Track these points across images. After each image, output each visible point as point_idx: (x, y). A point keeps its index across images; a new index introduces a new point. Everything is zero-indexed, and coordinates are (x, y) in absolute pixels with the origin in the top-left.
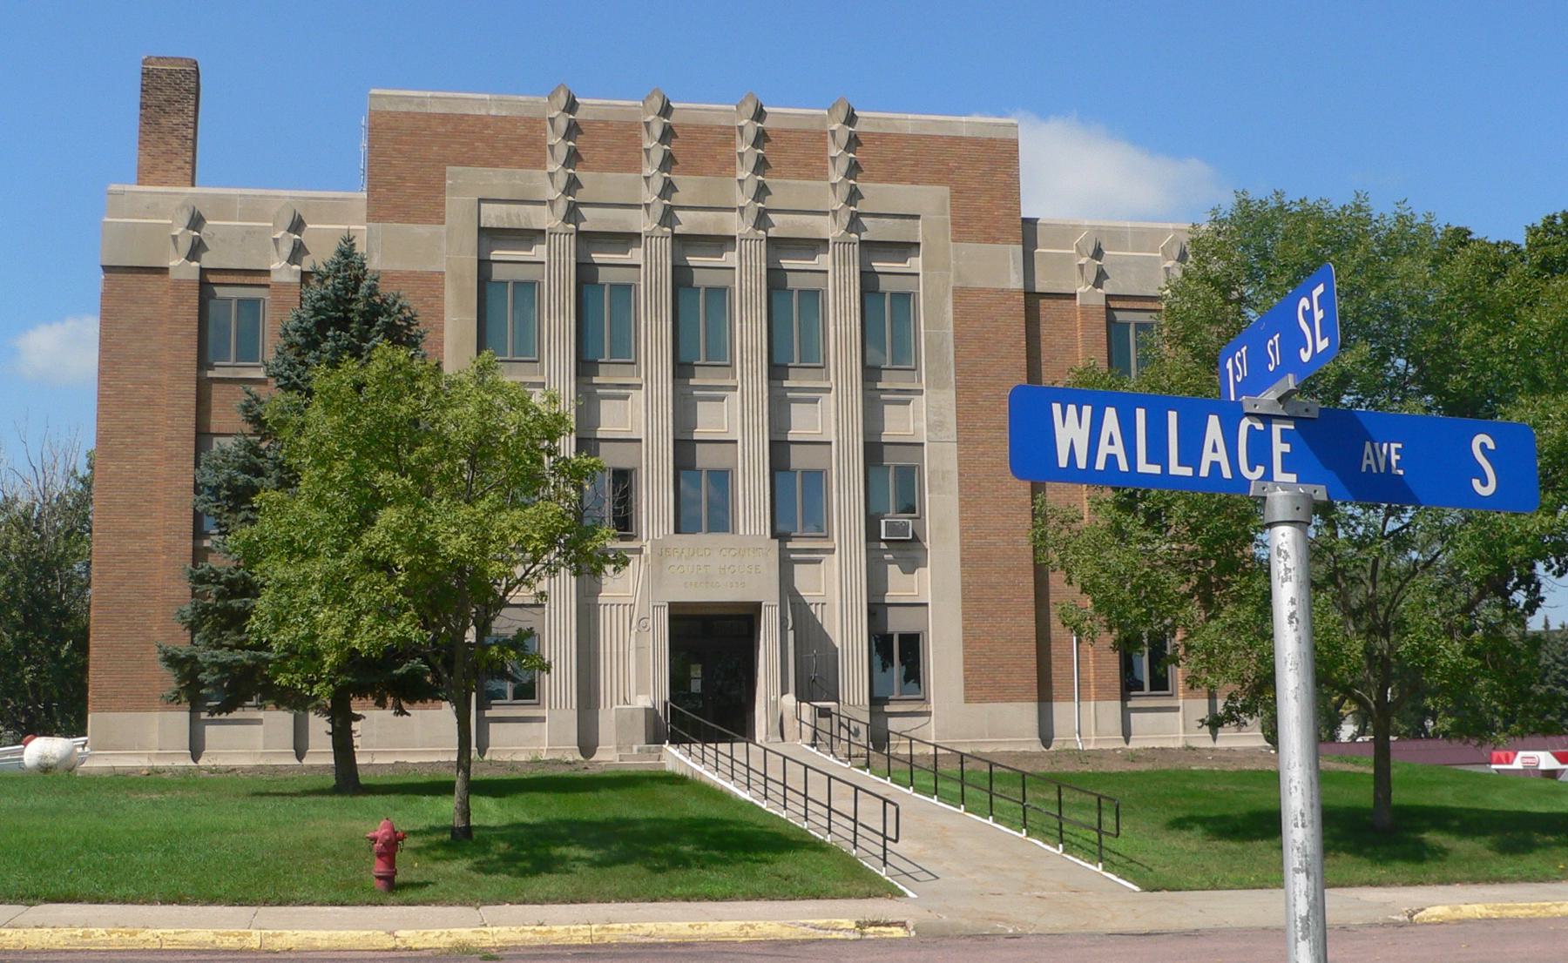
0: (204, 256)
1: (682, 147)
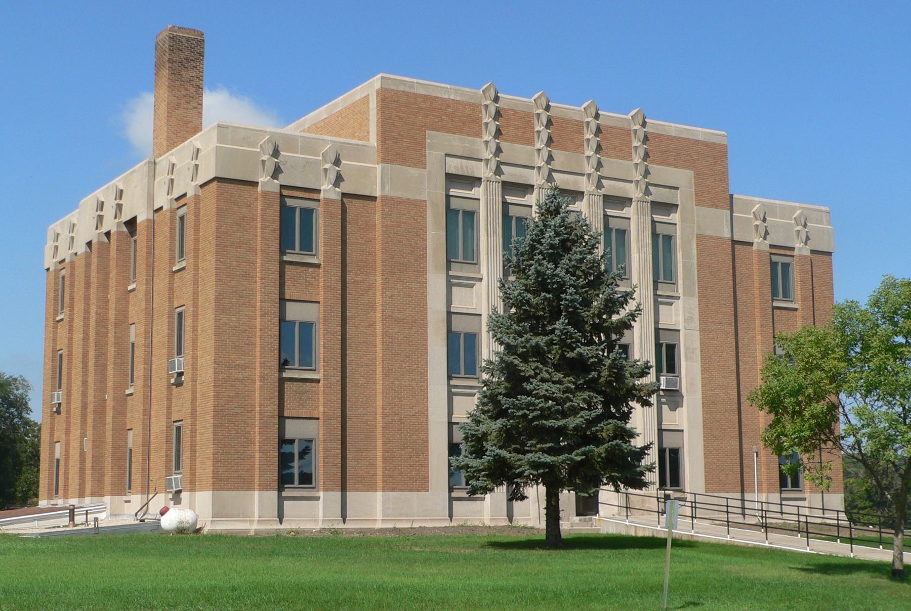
0: (281, 176)
1: (561, 133)
